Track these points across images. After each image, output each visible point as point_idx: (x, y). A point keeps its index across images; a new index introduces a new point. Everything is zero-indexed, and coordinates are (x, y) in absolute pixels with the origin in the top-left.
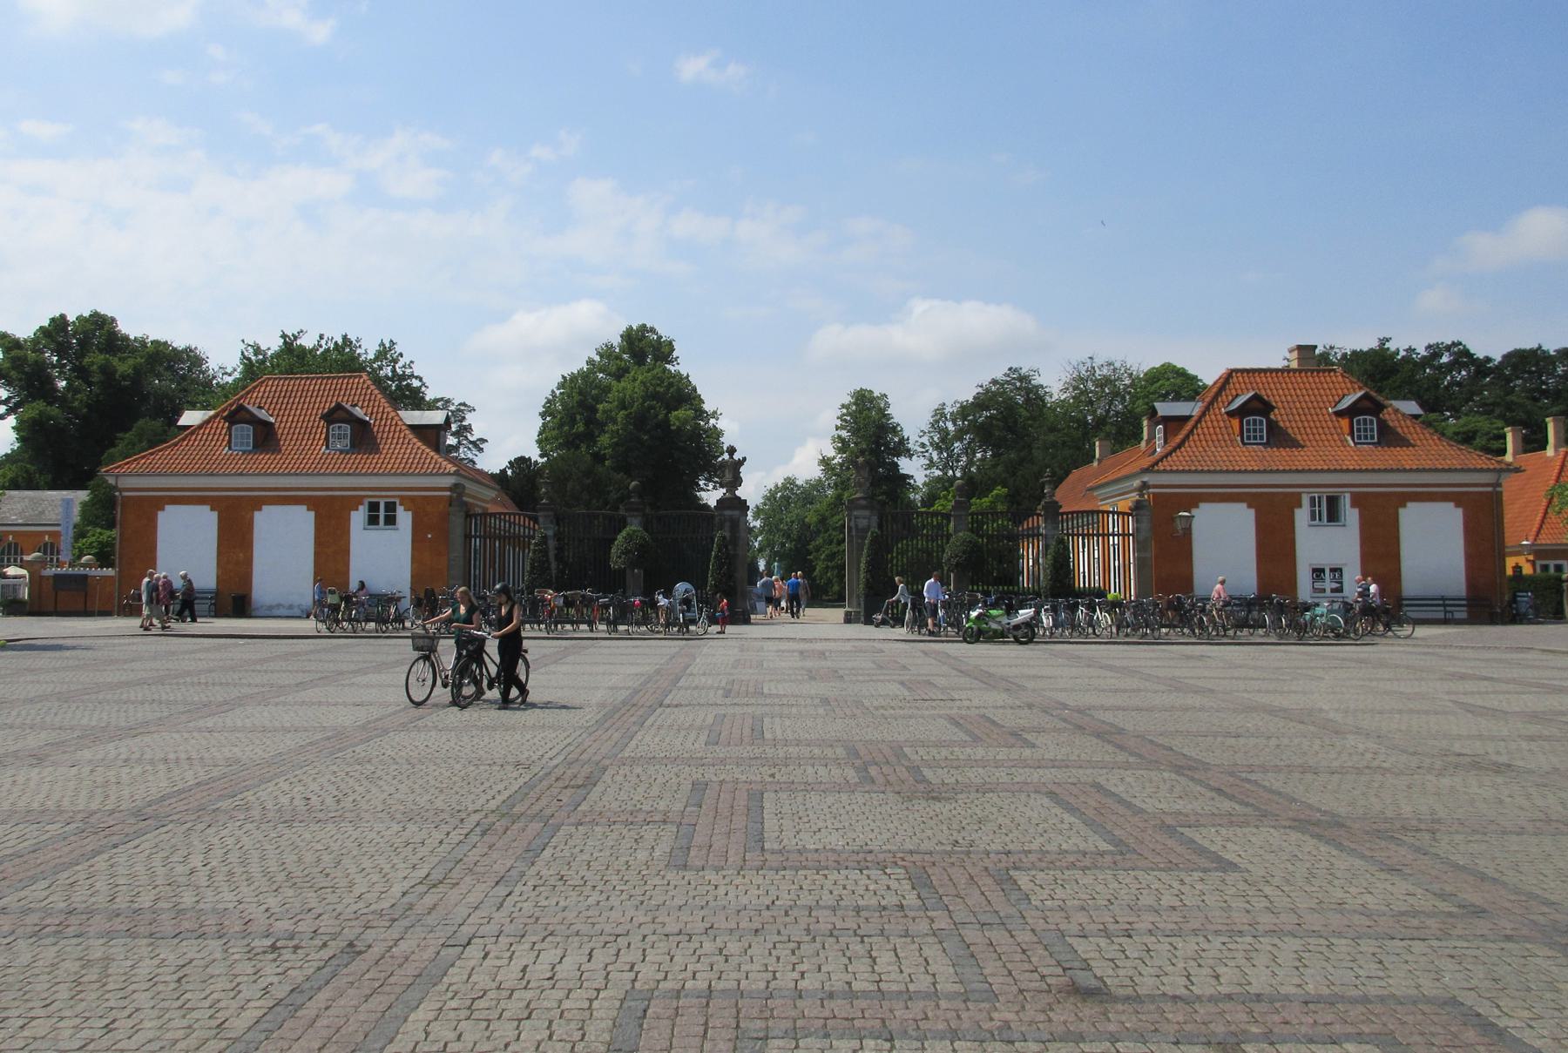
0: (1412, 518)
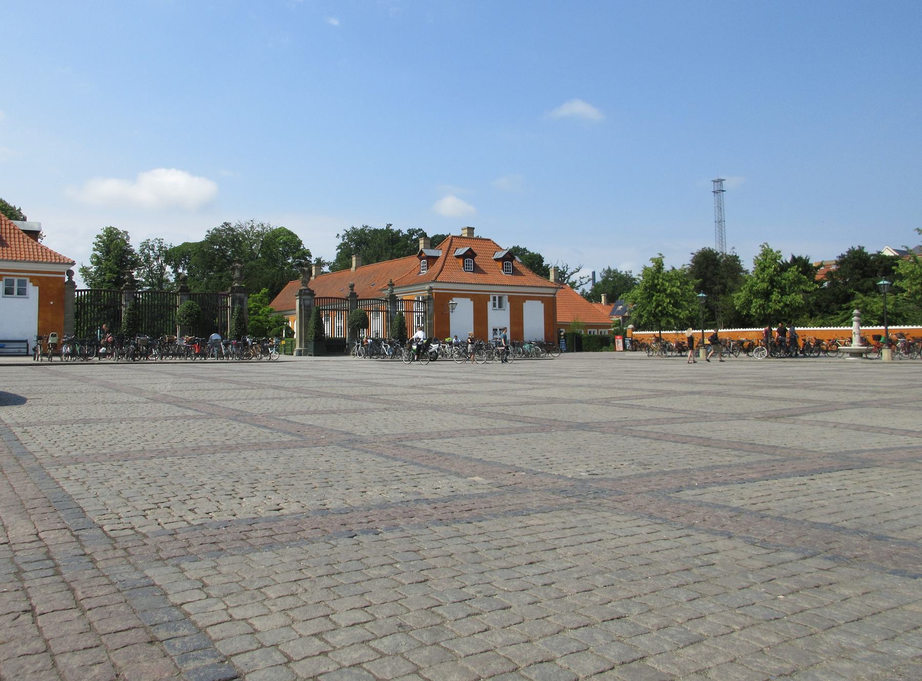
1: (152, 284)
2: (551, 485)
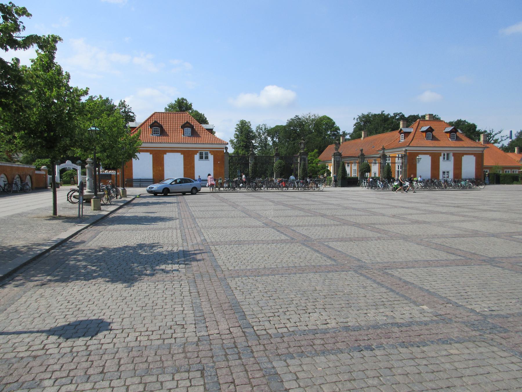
0: (168, 157)
1: (262, 147)
2: (466, 318)
